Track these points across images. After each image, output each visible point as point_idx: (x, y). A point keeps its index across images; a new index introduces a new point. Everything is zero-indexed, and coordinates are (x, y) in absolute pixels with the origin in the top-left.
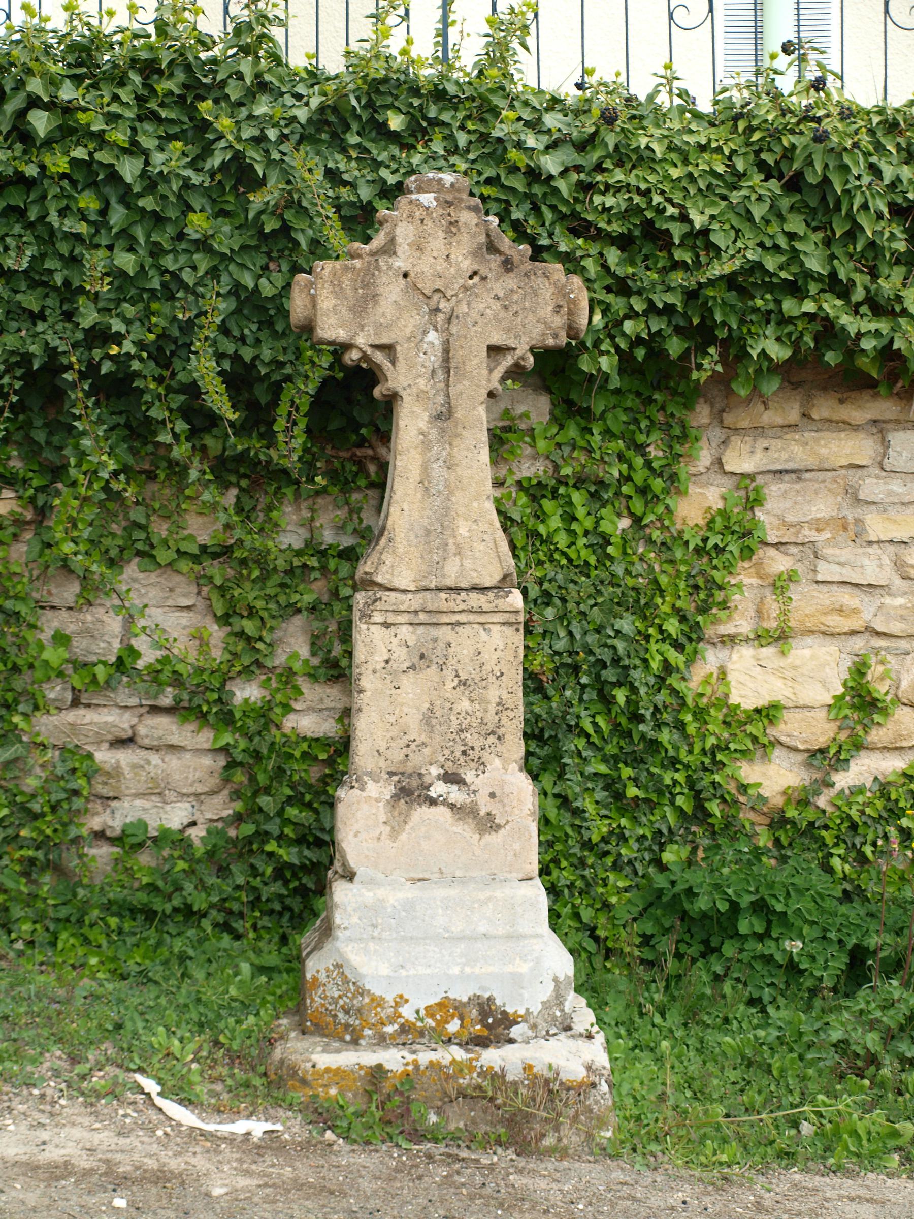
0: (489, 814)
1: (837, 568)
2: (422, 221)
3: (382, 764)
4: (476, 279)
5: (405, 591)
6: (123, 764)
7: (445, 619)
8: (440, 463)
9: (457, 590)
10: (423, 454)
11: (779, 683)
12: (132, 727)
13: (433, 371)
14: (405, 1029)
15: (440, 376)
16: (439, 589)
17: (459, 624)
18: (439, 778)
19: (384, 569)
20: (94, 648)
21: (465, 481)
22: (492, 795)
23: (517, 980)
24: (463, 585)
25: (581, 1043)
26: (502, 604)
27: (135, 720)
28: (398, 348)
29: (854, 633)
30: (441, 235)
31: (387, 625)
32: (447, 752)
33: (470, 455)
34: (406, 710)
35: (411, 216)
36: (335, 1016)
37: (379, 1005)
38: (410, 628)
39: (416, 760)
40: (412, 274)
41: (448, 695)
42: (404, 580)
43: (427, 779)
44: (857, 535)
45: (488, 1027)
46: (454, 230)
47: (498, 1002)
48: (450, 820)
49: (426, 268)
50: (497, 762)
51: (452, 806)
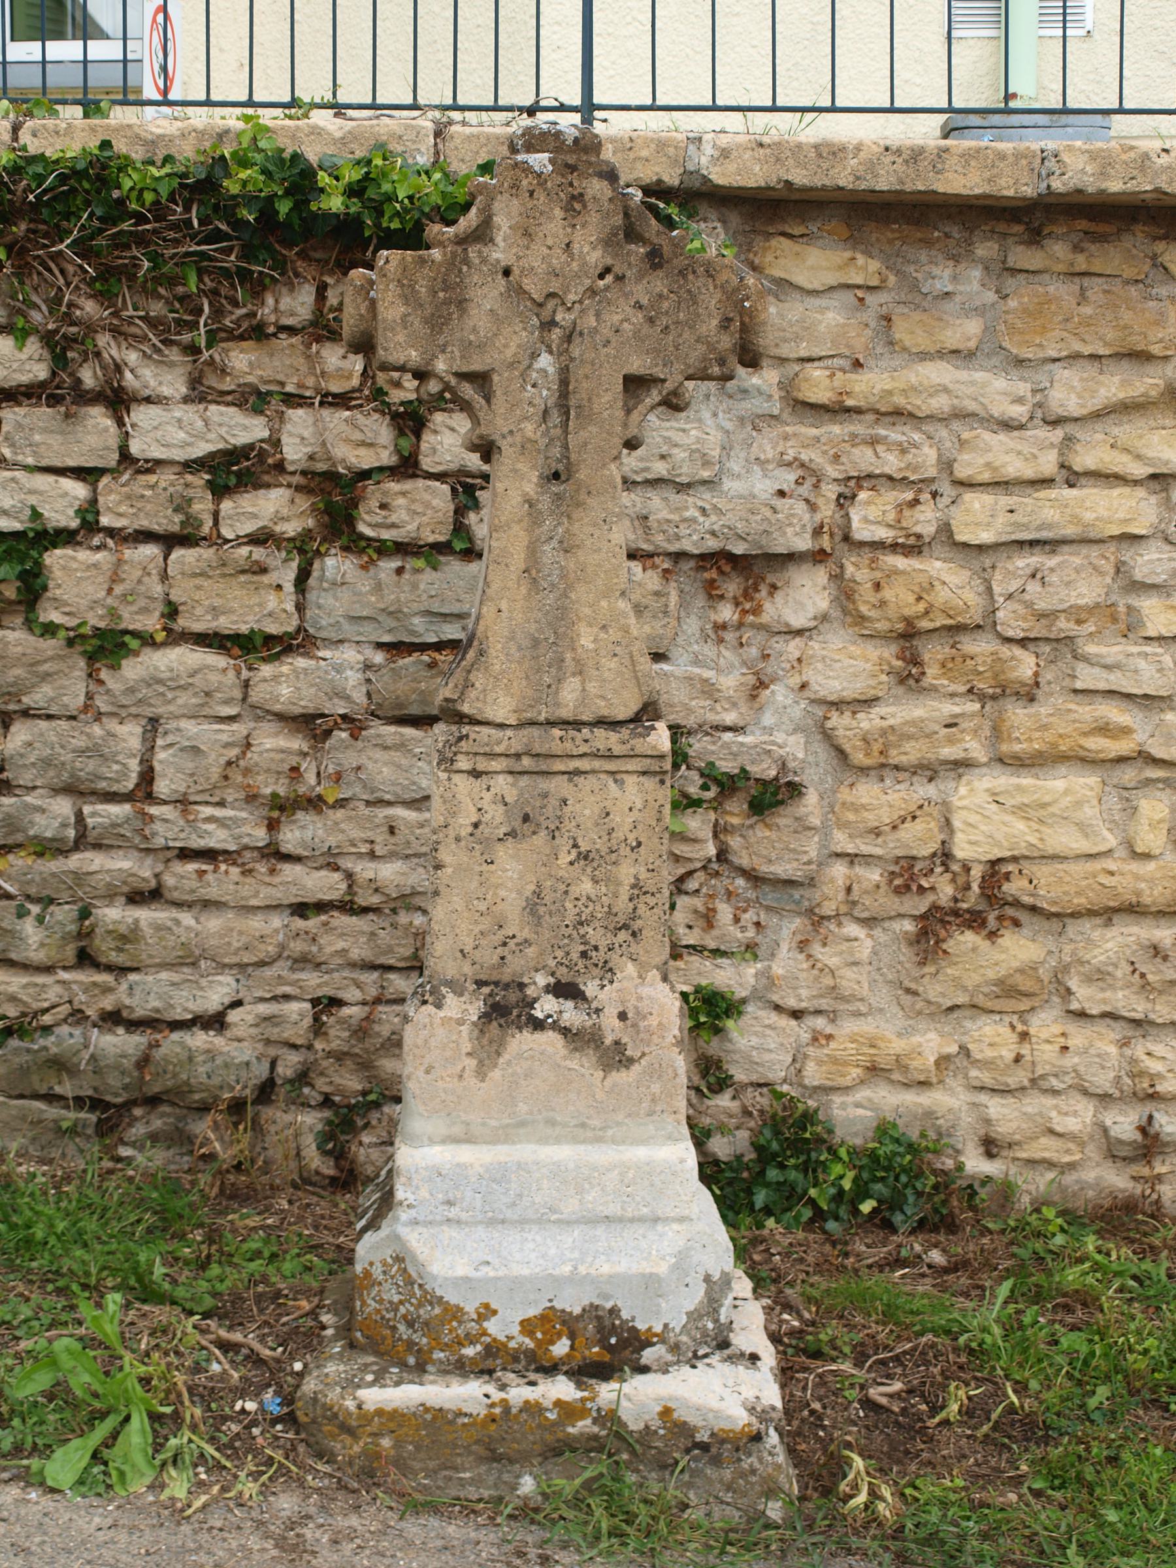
0: (617, 1043)
1: (1105, 674)
2: (531, 193)
3: (467, 969)
4: (609, 279)
5: (502, 726)
6: (143, 924)
7: (559, 766)
9: (577, 724)
11: (1021, 825)
12: (157, 876)
13: (546, 412)
14: (493, 1350)
15: (555, 418)
16: (551, 723)
17: (578, 772)
18: (548, 989)
19: (472, 694)
20: (104, 770)
21: (589, 570)
22: (623, 1016)
23: (650, 1284)
24: (585, 718)
25: (741, 1371)
26: (640, 745)
27: (160, 867)
28: (496, 378)
29: (1121, 760)
30: (558, 213)
31: (476, 774)
32: (560, 954)
33: (597, 533)
34: (502, 893)
35: (515, 186)
36: (394, 1328)
37: (454, 1317)
38: (510, 779)
39: (515, 965)
40: (516, 271)
41: (561, 873)
42: (501, 708)
43: (531, 991)
44: (1130, 627)
45: (610, 1349)
46: (578, 206)
47: (625, 1315)
48: (563, 1052)
49: (537, 263)
50: (631, 968)
51: (565, 1031)
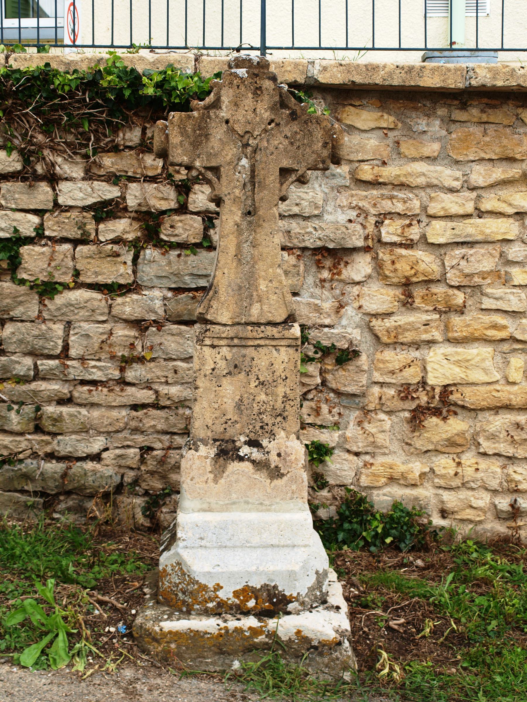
0: (276, 467)
1: (495, 302)
2: (238, 87)
3: (209, 434)
4: (273, 125)
5: (225, 325)
7: (250, 343)
8: (248, 243)
9: (259, 324)
10: (237, 238)
11: (457, 369)
13: (245, 185)
14: (221, 604)
15: (249, 187)
17: (259, 346)
18: (246, 443)
19: (212, 311)
21: (264, 255)
22: (279, 455)
23: (292, 575)
24: (262, 321)
25: (332, 614)
26: (287, 334)
27: (72, 388)
28: (222, 169)
29: (502, 340)
30: (250, 95)
31: (213, 346)
32: (251, 427)
33: (268, 239)
34: (225, 400)
36: (177, 595)
37: (204, 590)
38: (228, 349)
39: (231, 432)
40: (231, 121)
41: (252, 391)
42: (225, 317)
43: (238, 444)
46: (259, 92)
47: (280, 589)
48: (252, 471)
49: (241, 118)
50: (283, 434)
51: (253, 462)
